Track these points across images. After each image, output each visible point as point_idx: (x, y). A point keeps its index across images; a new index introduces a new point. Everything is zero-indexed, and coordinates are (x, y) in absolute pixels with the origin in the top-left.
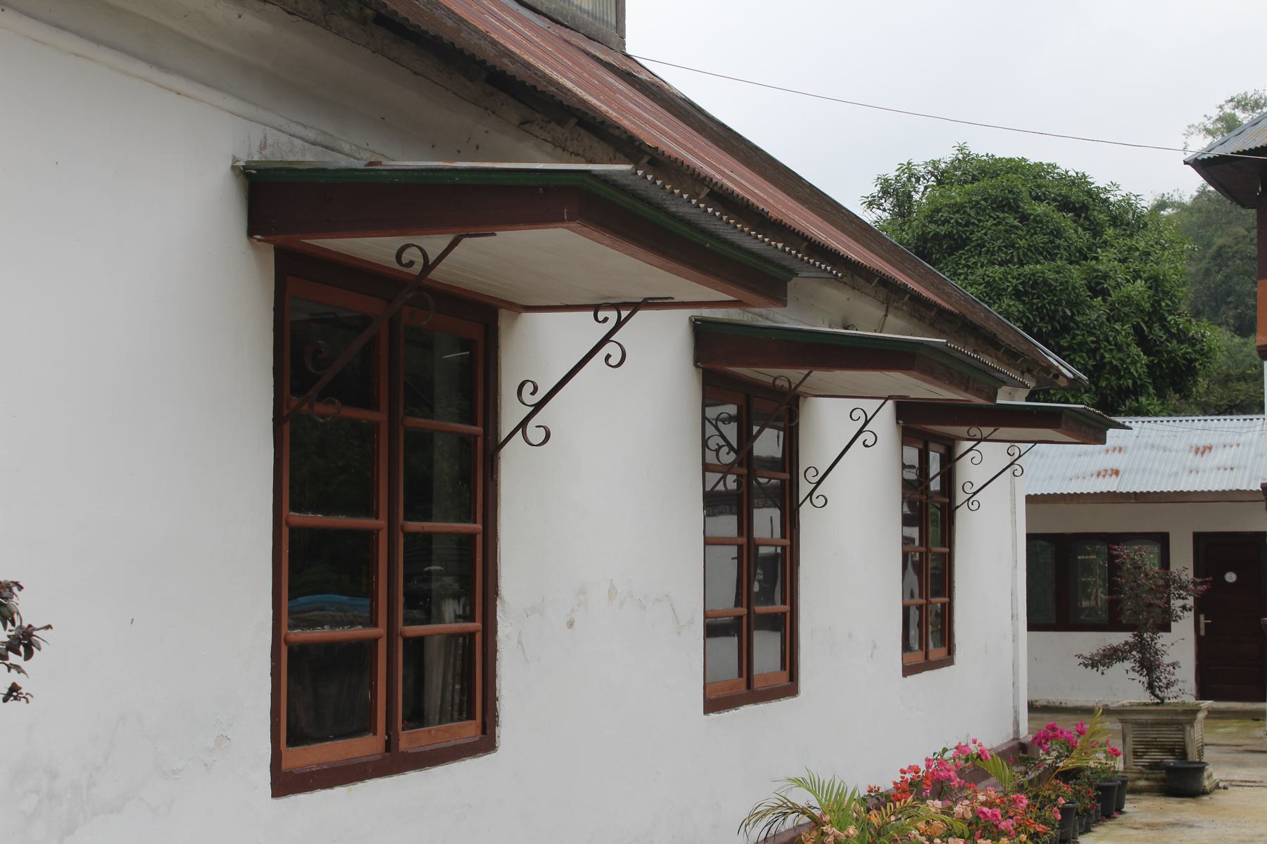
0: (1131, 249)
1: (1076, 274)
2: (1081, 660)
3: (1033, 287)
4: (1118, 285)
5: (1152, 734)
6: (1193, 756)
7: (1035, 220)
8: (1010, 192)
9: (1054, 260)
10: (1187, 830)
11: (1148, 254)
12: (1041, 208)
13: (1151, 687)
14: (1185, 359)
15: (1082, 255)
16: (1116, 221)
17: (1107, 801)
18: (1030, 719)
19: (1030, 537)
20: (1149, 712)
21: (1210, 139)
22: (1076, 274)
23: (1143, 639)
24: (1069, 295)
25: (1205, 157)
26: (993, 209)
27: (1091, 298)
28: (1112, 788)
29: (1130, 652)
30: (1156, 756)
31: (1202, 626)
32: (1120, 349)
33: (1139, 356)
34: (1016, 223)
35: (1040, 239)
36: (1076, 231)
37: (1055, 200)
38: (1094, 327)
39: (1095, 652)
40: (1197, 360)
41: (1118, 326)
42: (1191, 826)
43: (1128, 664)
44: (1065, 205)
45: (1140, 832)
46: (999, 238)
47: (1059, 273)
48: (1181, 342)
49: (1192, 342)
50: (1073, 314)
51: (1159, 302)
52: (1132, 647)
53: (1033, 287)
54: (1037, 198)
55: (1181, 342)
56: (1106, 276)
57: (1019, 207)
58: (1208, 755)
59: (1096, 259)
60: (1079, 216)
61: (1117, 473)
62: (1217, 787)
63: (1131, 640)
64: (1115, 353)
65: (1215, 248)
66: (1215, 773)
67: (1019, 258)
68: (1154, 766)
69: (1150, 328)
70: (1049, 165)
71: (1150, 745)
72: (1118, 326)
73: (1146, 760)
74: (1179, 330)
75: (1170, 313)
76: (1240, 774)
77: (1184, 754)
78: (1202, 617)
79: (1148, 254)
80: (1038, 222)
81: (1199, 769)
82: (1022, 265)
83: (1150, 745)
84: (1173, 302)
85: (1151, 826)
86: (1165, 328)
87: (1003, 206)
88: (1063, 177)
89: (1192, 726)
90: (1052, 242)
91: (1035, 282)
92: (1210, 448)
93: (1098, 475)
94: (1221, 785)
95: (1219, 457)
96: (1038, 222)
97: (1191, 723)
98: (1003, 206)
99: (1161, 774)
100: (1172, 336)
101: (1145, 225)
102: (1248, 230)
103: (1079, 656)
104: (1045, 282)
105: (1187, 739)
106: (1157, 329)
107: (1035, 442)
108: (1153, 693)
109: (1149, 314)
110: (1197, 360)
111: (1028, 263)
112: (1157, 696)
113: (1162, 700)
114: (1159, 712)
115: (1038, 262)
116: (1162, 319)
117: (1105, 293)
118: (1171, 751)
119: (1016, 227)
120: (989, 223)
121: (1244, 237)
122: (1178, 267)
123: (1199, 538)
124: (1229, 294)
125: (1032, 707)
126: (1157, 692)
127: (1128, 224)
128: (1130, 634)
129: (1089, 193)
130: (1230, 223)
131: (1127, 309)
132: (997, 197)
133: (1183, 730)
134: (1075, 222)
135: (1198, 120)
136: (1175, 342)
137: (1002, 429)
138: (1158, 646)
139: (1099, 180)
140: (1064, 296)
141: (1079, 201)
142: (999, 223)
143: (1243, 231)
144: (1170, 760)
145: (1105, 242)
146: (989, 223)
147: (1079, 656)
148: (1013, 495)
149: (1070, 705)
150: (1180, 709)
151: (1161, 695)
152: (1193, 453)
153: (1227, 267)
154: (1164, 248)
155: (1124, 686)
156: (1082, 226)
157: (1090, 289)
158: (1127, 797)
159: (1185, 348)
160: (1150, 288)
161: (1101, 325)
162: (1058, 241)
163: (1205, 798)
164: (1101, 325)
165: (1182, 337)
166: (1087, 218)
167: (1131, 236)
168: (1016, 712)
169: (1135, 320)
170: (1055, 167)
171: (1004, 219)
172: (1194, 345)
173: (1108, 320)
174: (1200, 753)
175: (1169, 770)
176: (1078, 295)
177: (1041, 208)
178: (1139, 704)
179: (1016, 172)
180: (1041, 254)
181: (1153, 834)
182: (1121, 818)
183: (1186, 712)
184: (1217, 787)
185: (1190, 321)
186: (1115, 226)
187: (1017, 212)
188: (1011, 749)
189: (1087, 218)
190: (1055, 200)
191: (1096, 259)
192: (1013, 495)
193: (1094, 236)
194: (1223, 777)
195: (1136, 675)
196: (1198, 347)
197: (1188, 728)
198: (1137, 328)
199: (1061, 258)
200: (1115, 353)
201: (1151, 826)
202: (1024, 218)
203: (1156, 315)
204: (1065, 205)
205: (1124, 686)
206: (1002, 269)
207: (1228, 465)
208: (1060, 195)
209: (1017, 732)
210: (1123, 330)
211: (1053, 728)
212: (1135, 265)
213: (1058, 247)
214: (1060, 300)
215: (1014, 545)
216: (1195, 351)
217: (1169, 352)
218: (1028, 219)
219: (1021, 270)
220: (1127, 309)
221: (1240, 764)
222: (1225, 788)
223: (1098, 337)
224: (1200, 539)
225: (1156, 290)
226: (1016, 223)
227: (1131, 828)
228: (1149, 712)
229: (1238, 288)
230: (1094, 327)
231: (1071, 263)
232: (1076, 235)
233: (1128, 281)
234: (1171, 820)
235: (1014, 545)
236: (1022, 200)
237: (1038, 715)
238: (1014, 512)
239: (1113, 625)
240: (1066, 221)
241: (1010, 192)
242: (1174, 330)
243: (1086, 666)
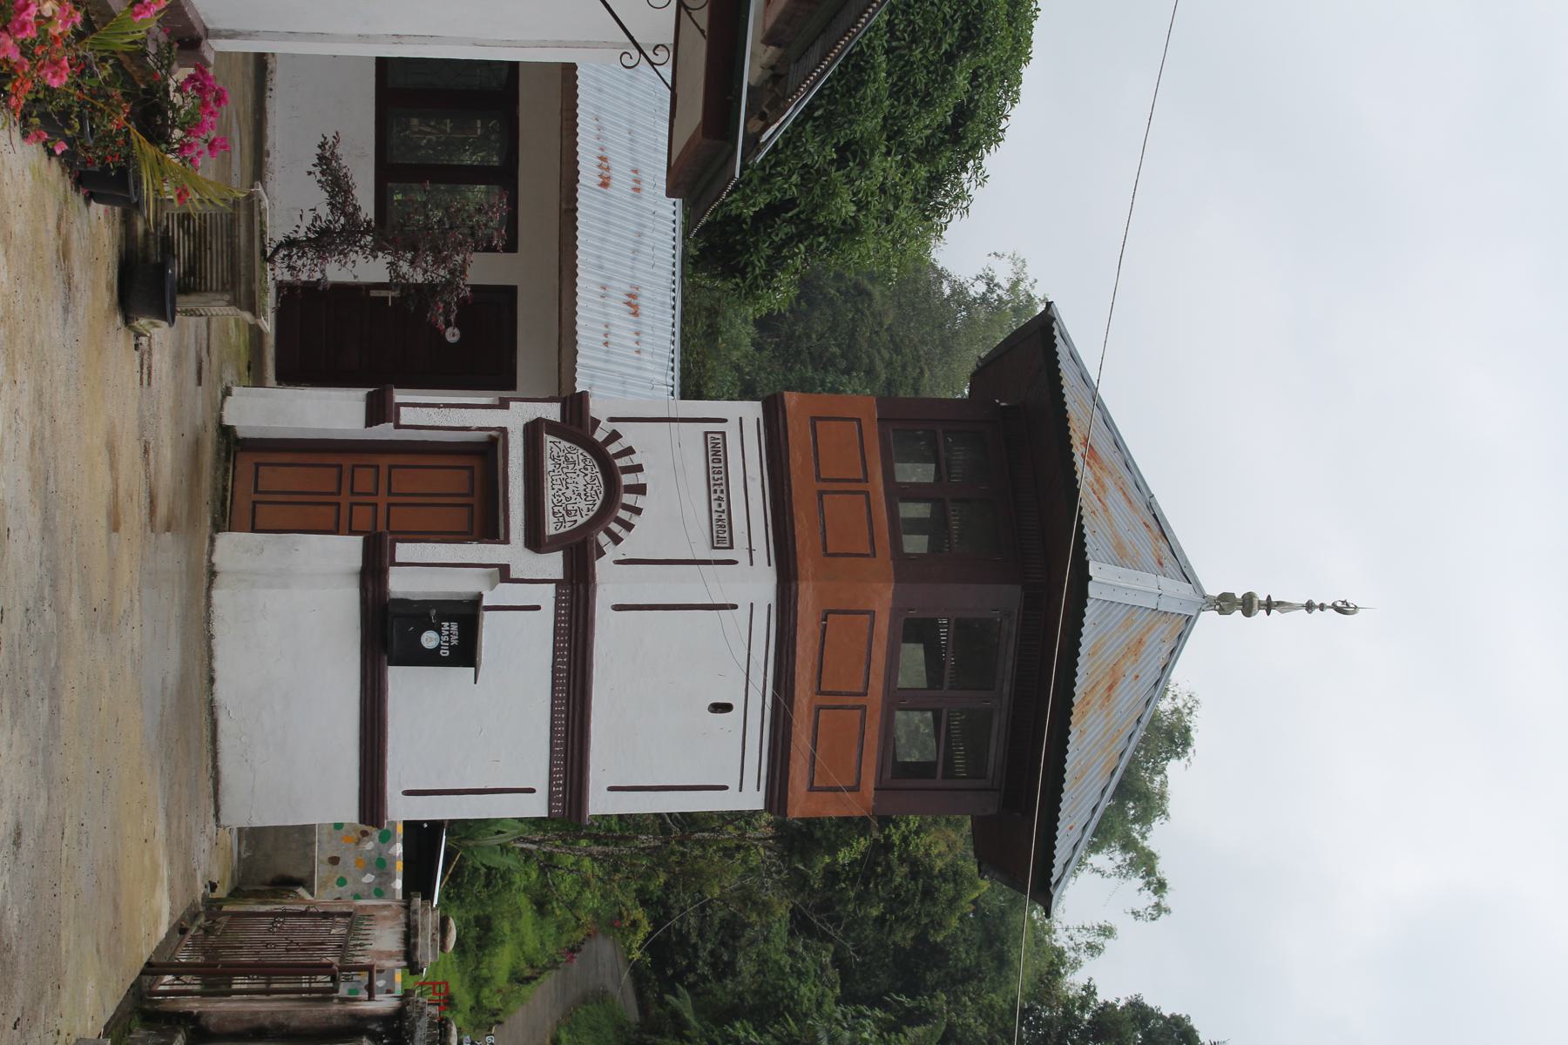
0: (897, 200)
1: (870, 124)
2: (330, 140)
3: (856, 66)
4: (851, 181)
5: (217, 244)
6: (183, 302)
7: (946, 72)
8: (987, 39)
9: (890, 96)
10: (58, 306)
11: (888, 221)
12: (962, 81)
13: (290, 243)
14: (746, 265)
15: (894, 131)
16: (936, 181)
17: (101, 179)
18: (246, 54)
19: (514, 66)
20: (251, 240)
21: (1006, 285)
22: (870, 124)
23: (363, 234)
24: (842, 115)
25: (1056, 333)
26: (965, 17)
27: (835, 145)
28: (126, 188)
29: (344, 213)
30: (183, 247)
31: (383, 293)
32: (765, 180)
33: (754, 205)
34: (945, 47)
35: (921, 78)
36: (927, 127)
37: (971, 99)
38: (796, 147)
39: (343, 163)
40: (744, 279)
41: (795, 178)
42: (66, 310)
43: (324, 211)
44: (963, 113)
45: (53, 233)
46: (925, 22)
47: (873, 102)
48: (769, 260)
49: (768, 275)
50: (815, 119)
51: (825, 233)
52: (352, 217)
53: (856, 66)
54: (975, 76)
55: (769, 260)
56: (864, 165)
57: (966, 51)
58: (190, 325)
59: (888, 153)
60: (945, 133)
61: (605, 185)
62: (138, 335)
63: (362, 216)
64: (760, 173)
65: (870, 287)
66: (160, 334)
67: (897, 48)
68: (167, 245)
69: (790, 221)
70: (1017, 93)
71: (199, 239)
72: (795, 178)
73: (177, 233)
74: (786, 258)
75: (809, 249)
76: (161, 362)
77: (186, 289)
78: (396, 294)
79: (888, 221)
80: (943, 76)
81: (163, 311)
82: (887, 52)
83: (199, 239)
84: (823, 252)
85: (64, 253)
86: (789, 240)
87: (968, 30)
88: (999, 113)
89: (230, 304)
90: (915, 94)
91: (862, 70)
92: (635, 314)
93: (601, 158)
94: (143, 340)
95: (618, 314)
96: (943, 76)
97: (234, 302)
98: (968, 30)
99: (155, 256)
100: (778, 249)
101: (928, 219)
102: (889, 329)
103: (336, 137)
104: (863, 83)
105: (210, 296)
106: (787, 230)
107: (673, 89)
108: (280, 246)
109: (809, 220)
110: (744, 279)
111: (889, 60)
112: (276, 251)
113: (271, 260)
114: (251, 255)
115: (889, 74)
116: (801, 237)
117: (841, 163)
118: (193, 268)
119: (938, 47)
120: (947, 9)
121: (881, 324)
122: (867, 252)
123: (510, 293)
124: (810, 303)
125: (261, 63)
126: (283, 252)
127: (930, 196)
128: (371, 216)
129: (976, 146)
130: (900, 306)
131: (818, 191)
132: (982, 21)
133: (224, 290)
134: (939, 126)
135: (1031, 272)
136: (769, 252)
137: (702, 45)
138: (353, 256)
139: (993, 160)
140: (840, 109)
141: (967, 131)
142: (946, 23)
143: (887, 322)
144: (176, 270)
145: (909, 166)
146: (947, 9)
147: (336, 137)
148: (586, 45)
149: (269, 103)
150: (257, 286)
151: (277, 258)
152: (628, 289)
153: (846, 302)
154: (894, 242)
155: (291, 202)
156: (933, 135)
157: (848, 144)
158: (117, 209)
159: (760, 265)
160: (844, 223)
161: (798, 156)
162: (915, 102)
163: (119, 320)
164: (798, 156)
165: (776, 262)
166: (942, 142)
167: (915, 200)
168: (249, 35)
169: (802, 202)
170: (1014, 101)
171: (952, 30)
172: (764, 278)
173: (805, 165)
174: (189, 313)
175: (162, 268)
176: (840, 127)
177: (962, 81)
178: (262, 223)
179: (1014, 49)
180: (900, 79)
181: (50, 254)
182: (78, 200)
183: (251, 295)
184: (138, 335)
185: (796, 272)
186: (929, 180)
187: (959, 48)
188: (190, 26)
189: (942, 142)
190: (971, 99)
191: (888, 153)
192: (586, 45)
193: (918, 151)
194: (156, 339)
195: (308, 220)
196: (762, 283)
197: (227, 297)
198: (792, 203)
199: (892, 106)
200: (760, 173)
201: (64, 253)
202: (951, 57)
203: (807, 229)
204: (963, 113)
205: (291, 202)
206: (883, 25)
207: (611, 339)
208: (977, 107)
209: (218, 35)
210: (790, 186)
211: (220, 99)
212: (876, 204)
213: (908, 102)
214: (835, 102)
215: (510, 44)
216: (756, 278)
217: (756, 244)
218: (948, 62)
219: (880, 50)
220: (818, 191)
221: (178, 359)
222: (136, 347)
223: (782, 151)
224: (508, 294)
225: (841, 231)
226: (945, 47)
227: (60, 218)
228: (251, 240)
229: (817, 314)
230: (796, 147)
231: (885, 118)
232: (918, 131)
233: (855, 195)
234: (77, 275)
235: (510, 44)
236: (974, 55)
237: (251, 69)
238: (560, 45)
239: (387, 172)
240: (943, 113)
241: (987, 39)
242: (785, 252)
243: (322, 146)
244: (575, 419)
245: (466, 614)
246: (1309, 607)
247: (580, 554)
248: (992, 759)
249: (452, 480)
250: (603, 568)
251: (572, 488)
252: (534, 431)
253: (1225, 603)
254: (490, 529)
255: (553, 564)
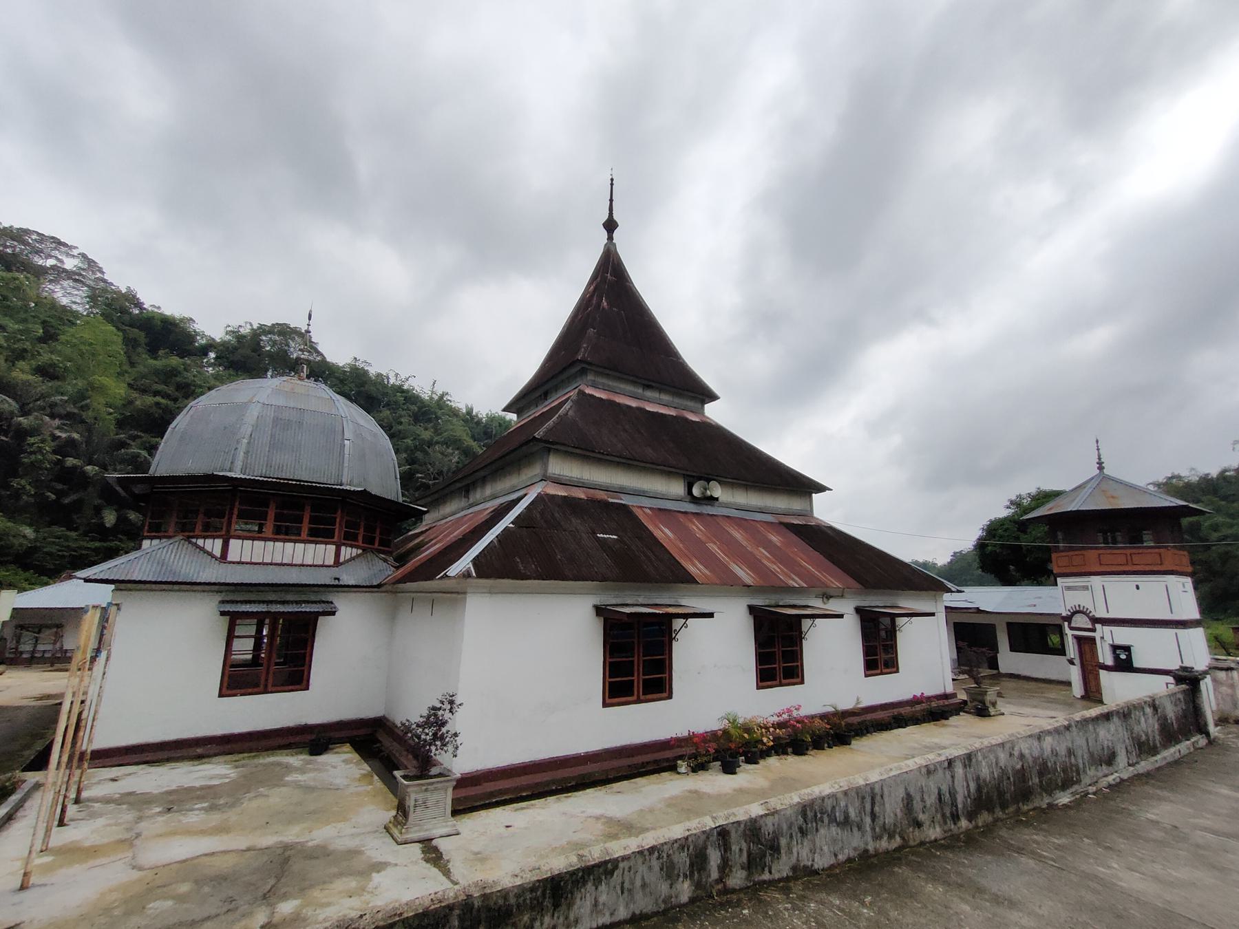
244: (1068, 619)
245: (1115, 648)
246: (610, 226)
247: (1095, 620)
248: (744, 543)
249: (1087, 648)
250: (1097, 616)
251: (1080, 621)
252: (1072, 628)
253: (1101, 468)
254: (1093, 640)
255: (1098, 626)
